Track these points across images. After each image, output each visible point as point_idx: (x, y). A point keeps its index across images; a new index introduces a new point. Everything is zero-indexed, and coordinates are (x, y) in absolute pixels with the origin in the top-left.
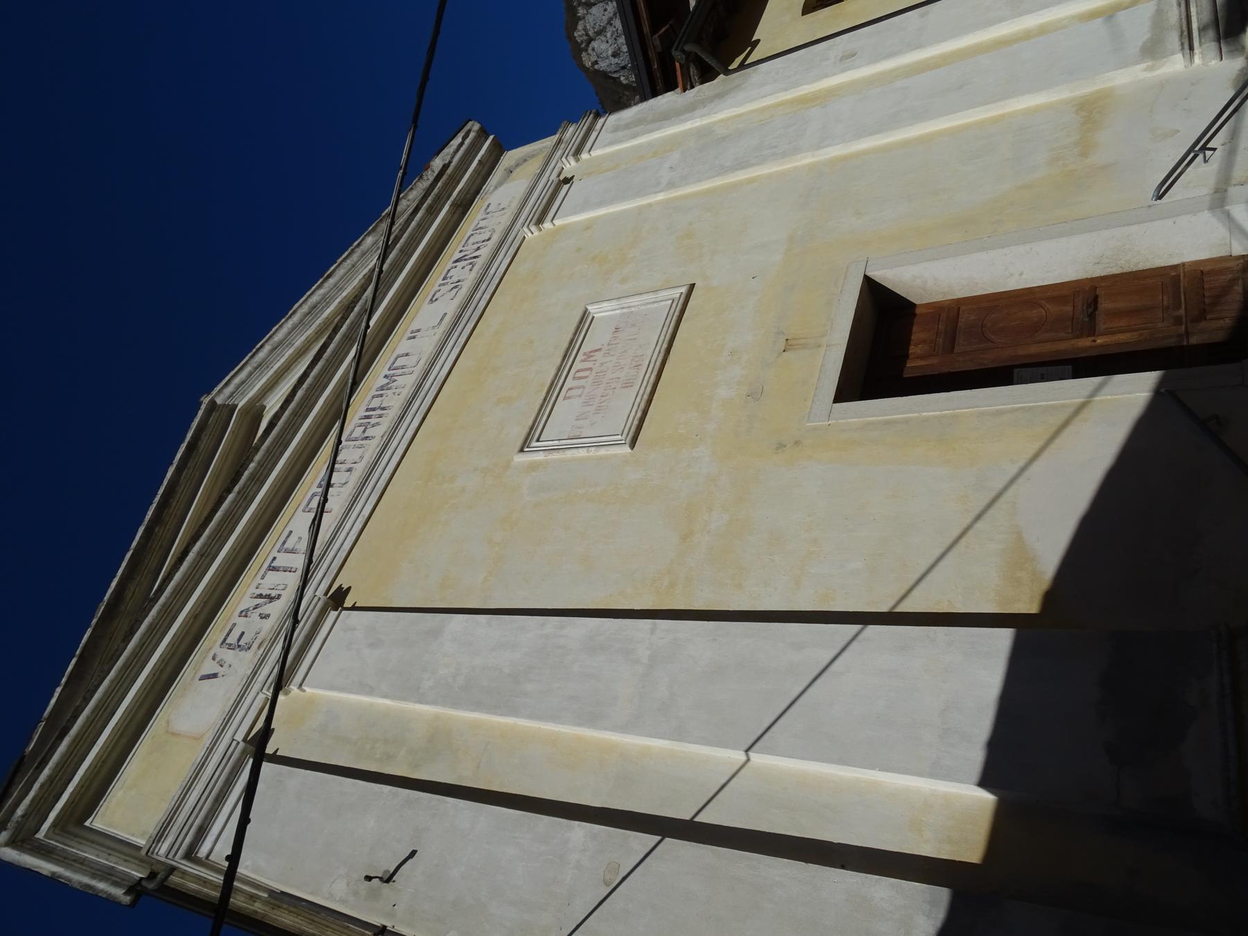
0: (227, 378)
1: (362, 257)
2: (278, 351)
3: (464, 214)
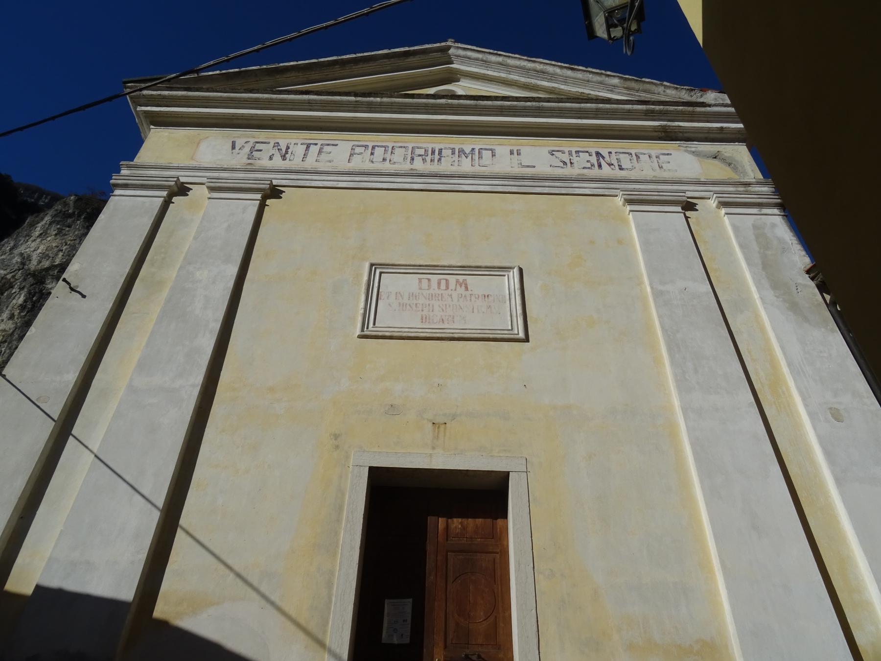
0: (469, 47)
1: (599, 83)
2: (501, 67)
3: (660, 139)
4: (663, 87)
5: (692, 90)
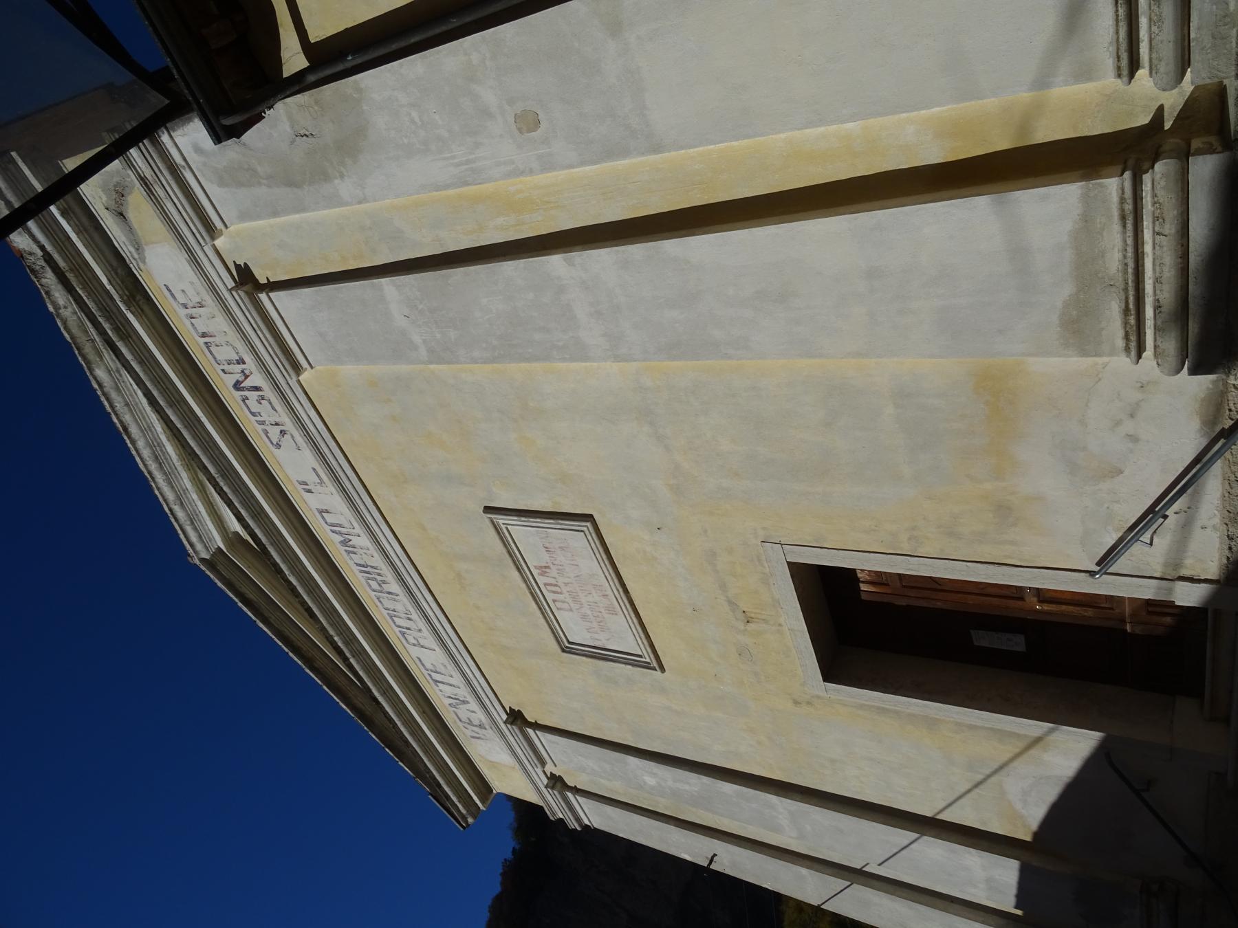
0: (185, 542)
4: (61, 311)
5: (33, 271)
